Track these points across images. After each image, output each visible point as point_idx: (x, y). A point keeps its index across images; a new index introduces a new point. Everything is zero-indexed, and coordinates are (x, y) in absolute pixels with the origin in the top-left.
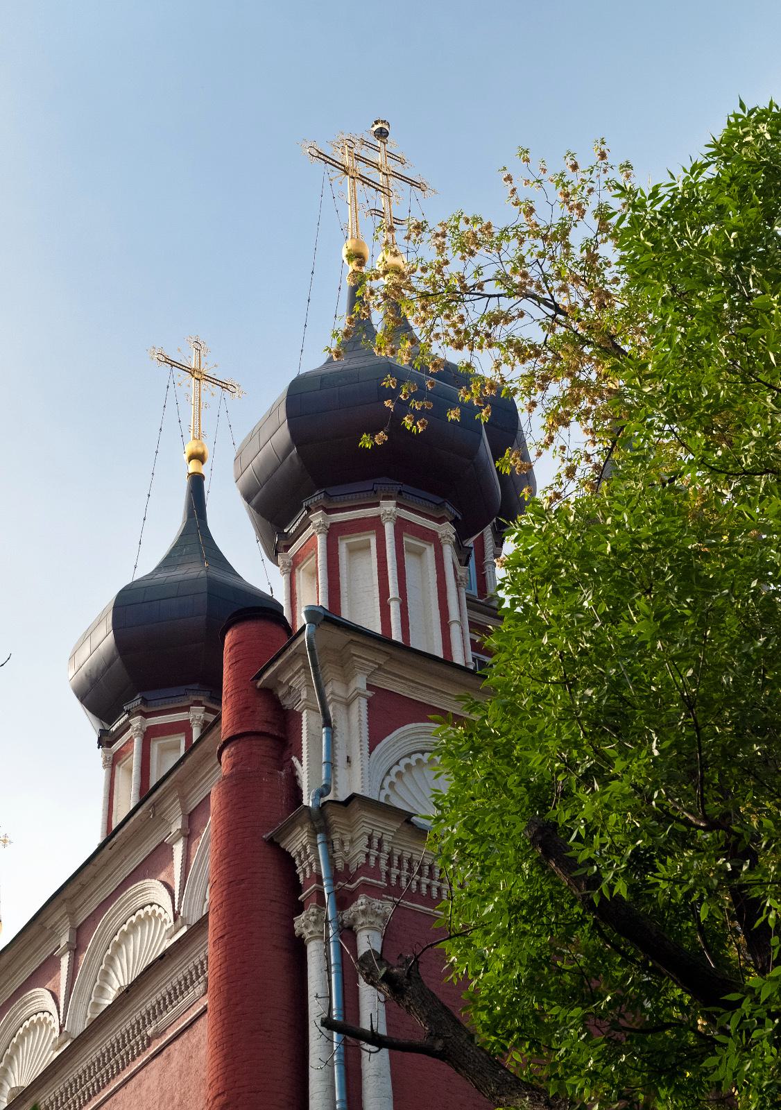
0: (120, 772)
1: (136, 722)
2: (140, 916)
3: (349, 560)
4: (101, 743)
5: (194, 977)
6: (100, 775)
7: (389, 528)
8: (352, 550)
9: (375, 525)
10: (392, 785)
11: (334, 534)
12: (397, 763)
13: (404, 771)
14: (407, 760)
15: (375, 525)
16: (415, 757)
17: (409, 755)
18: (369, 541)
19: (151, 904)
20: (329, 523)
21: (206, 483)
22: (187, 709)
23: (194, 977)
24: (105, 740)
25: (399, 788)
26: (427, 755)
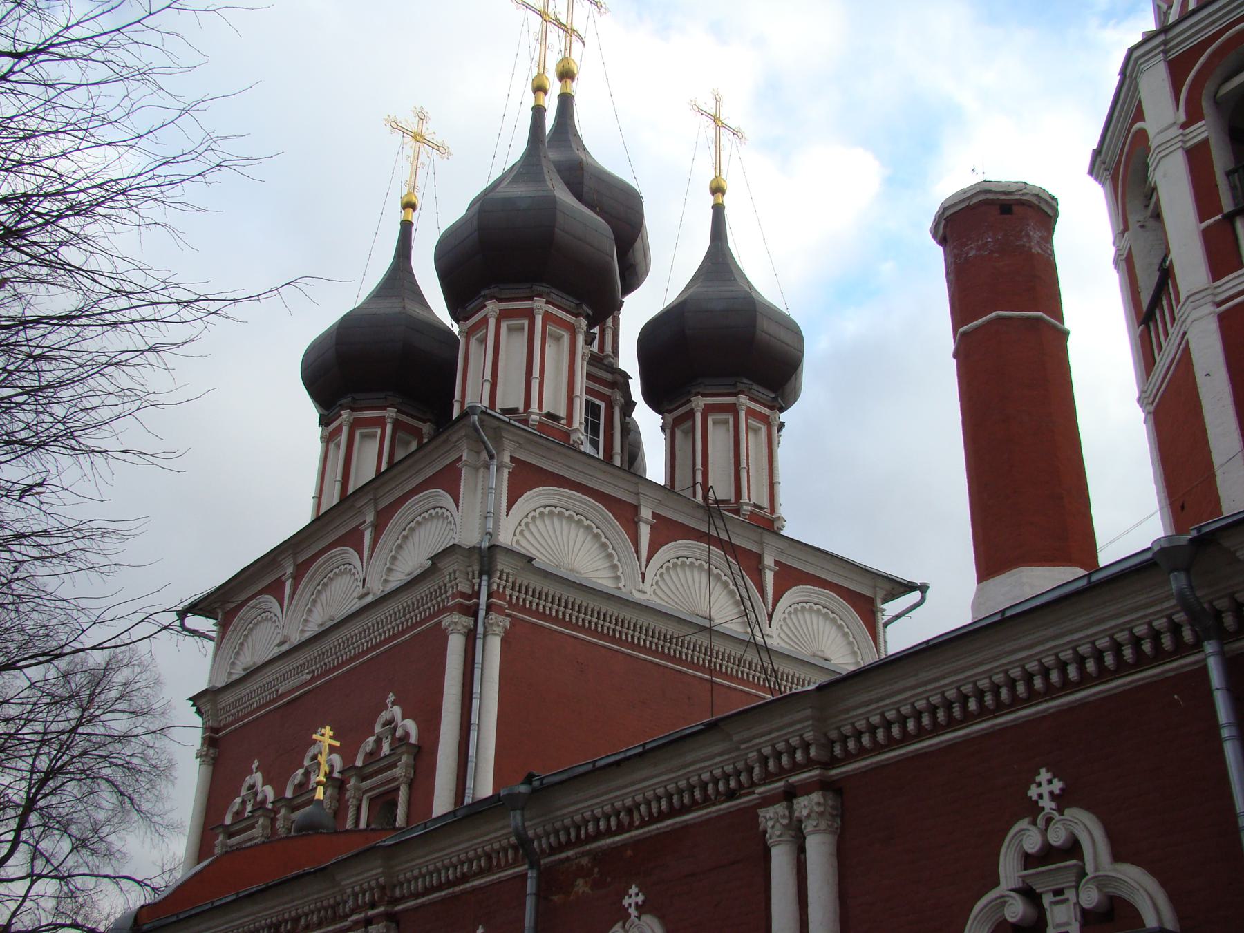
0: (332, 446)
1: (345, 414)
2: (431, 514)
3: (361, 443)
4: (321, 423)
5: (443, 591)
6: (317, 447)
7: (539, 320)
8: (364, 436)
9: (381, 422)
10: (534, 518)
11: (355, 425)
12: (535, 510)
13: (537, 516)
14: (542, 509)
15: (530, 314)
16: (548, 508)
17: (545, 507)
18: (377, 432)
19: (441, 508)
20: (352, 418)
21: (414, 229)
22: (384, 408)
23: (443, 591)
24: (324, 422)
25: (539, 522)
26: (558, 509)
